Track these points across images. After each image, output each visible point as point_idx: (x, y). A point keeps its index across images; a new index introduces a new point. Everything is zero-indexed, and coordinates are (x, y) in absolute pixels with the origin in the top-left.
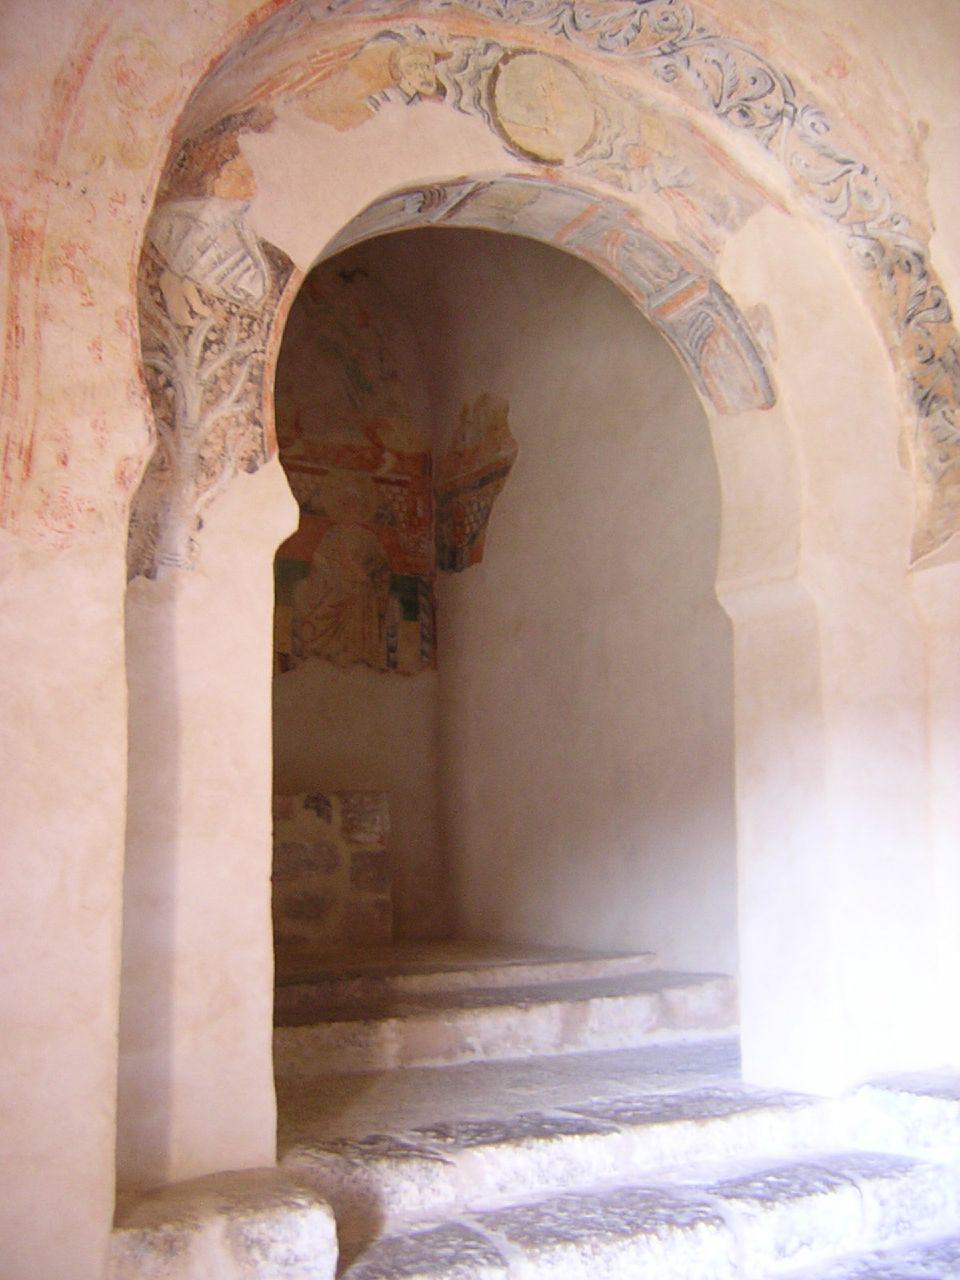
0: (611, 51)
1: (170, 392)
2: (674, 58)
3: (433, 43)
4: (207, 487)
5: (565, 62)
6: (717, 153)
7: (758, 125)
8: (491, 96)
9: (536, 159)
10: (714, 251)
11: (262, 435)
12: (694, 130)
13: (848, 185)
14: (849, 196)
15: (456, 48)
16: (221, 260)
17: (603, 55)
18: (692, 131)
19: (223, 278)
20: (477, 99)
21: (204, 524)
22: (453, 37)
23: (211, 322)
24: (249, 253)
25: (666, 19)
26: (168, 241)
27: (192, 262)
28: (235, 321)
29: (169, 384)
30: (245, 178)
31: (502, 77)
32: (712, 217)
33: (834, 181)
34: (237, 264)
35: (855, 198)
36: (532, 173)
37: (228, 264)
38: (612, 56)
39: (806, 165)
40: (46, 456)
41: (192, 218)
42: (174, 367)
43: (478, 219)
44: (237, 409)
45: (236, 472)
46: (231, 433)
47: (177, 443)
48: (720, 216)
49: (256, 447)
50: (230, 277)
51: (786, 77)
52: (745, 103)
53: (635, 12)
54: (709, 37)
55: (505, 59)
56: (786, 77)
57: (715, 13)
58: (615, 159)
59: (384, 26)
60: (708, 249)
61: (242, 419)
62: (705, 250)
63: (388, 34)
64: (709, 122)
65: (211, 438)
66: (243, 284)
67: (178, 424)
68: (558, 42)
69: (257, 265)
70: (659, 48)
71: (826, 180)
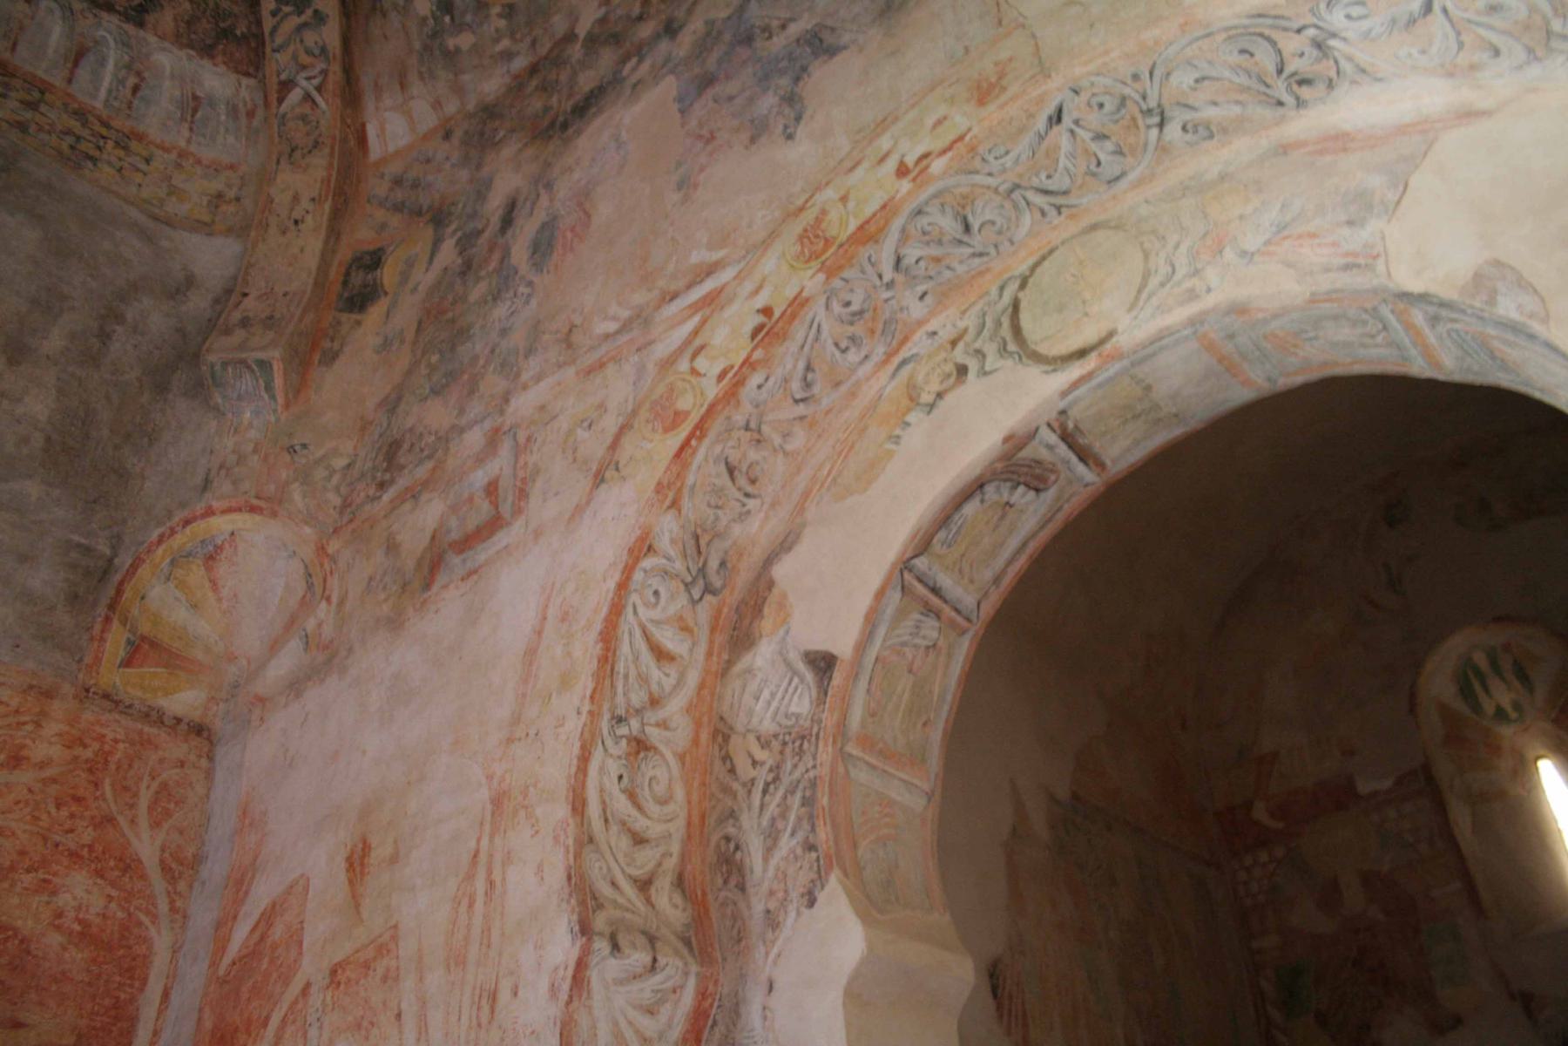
0: (1123, 174)
1: (738, 855)
2: (1172, 118)
3: (946, 334)
4: (773, 942)
5: (1094, 227)
6: (1339, 142)
7: (1333, 74)
8: (1017, 330)
9: (1082, 353)
10: (1370, 261)
11: (818, 860)
12: (1284, 149)
13: (1469, 21)
14: (1490, 27)
15: (970, 321)
16: (773, 695)
17: (1123, 184)
18: (1285, 153)
19: (776, 713)
20: (1003, 350)
21: (776, 986)
22: (964, 312)
23: (770, 762)
24: (795, 673)
25: (1101, 106)
26: (732, 706)
27: (751, 713)
28: (788, 750)
29: (737, 848)
30: (782, 605)
31: (1023, 305)
32: (1350, 223)
33: (1459, 34)
34: (786, 691)
35: (1495, 21)
36: (1084, 372)
37: (779, 695)
38: (1132, 176)
39: (1423, 52)
40: (504, 996)
41: (749, 671)
42: (740, 828)
43: (1137, 443)
44: (794, 842)
45: (799, 914)
46: (791, 871)
47: (749, 907)
48: (1360, 207)
49: (813, 875)
50: (783, 709)
51: (1253, 16)
52: (1285, 75)
53: (1072, 132)
54: (1151, 74)
55: (1023, 286)
56: (1253, 16)
57: (1114, 55)
58: (1181, 271)
59: (896, 360)
60: (1358, 266)
61: (799, 851)
62: (1355, 271)
63: (904, 362)
64: (1301, 125)
65: (775, 887)
66: (793, 709)
67: (748, 885)
68: (1072, 217)
69: (802, 680)
70: (1149, 127)
71: (1455, 47)
